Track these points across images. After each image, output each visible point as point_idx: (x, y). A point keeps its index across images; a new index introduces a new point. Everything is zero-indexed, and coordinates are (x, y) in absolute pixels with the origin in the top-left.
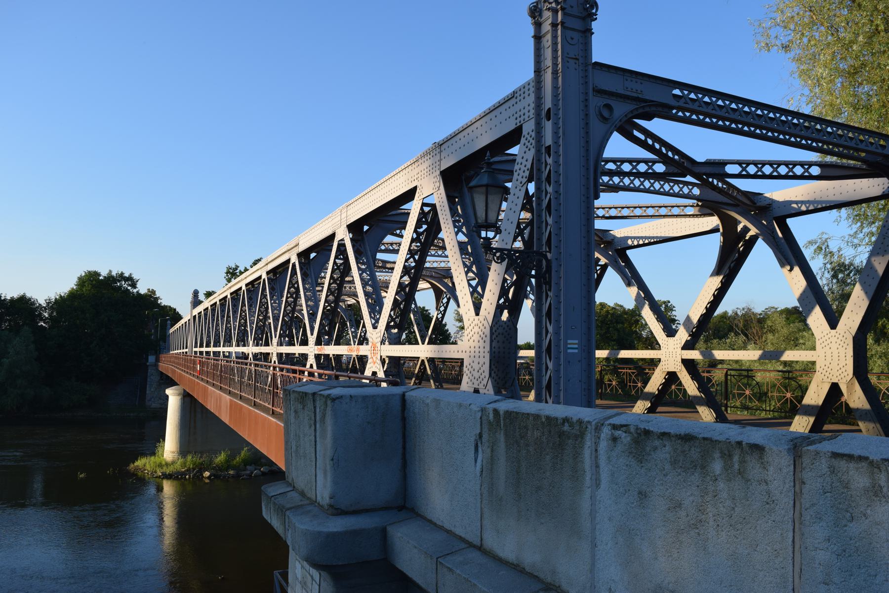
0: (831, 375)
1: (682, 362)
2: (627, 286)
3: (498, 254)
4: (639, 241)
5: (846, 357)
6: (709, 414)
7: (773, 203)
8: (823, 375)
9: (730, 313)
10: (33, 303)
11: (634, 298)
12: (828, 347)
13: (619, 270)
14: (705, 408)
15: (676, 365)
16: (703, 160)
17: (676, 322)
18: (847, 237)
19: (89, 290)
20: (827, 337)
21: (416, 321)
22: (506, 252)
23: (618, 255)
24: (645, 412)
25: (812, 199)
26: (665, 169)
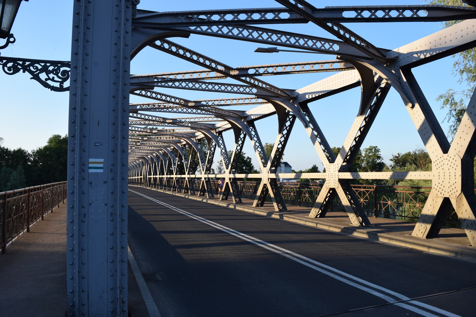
0: (444, 191)
1: (339, 181)
2: (305, 128)
3: (10, 65)
4: (313, 95)
5: (455, 176)
6: (356, 220)
7: (400, 56)
8: (437, 191)
9: (412, 153)
10: (25, 153)
11: (310, 136)
12: (441, 168)
13: (300, 117)
14: (353, 215)
15: (335, 183)
16: (323, 7)
17: (381, 158)
18: (466, 92)
19: (54, 145)
20: (440, 160)
21: (200, 157)
22: (21, 63)
23: (301, 107)
24: (318, 216)
25: (427, 48)
26: (289, 16)
